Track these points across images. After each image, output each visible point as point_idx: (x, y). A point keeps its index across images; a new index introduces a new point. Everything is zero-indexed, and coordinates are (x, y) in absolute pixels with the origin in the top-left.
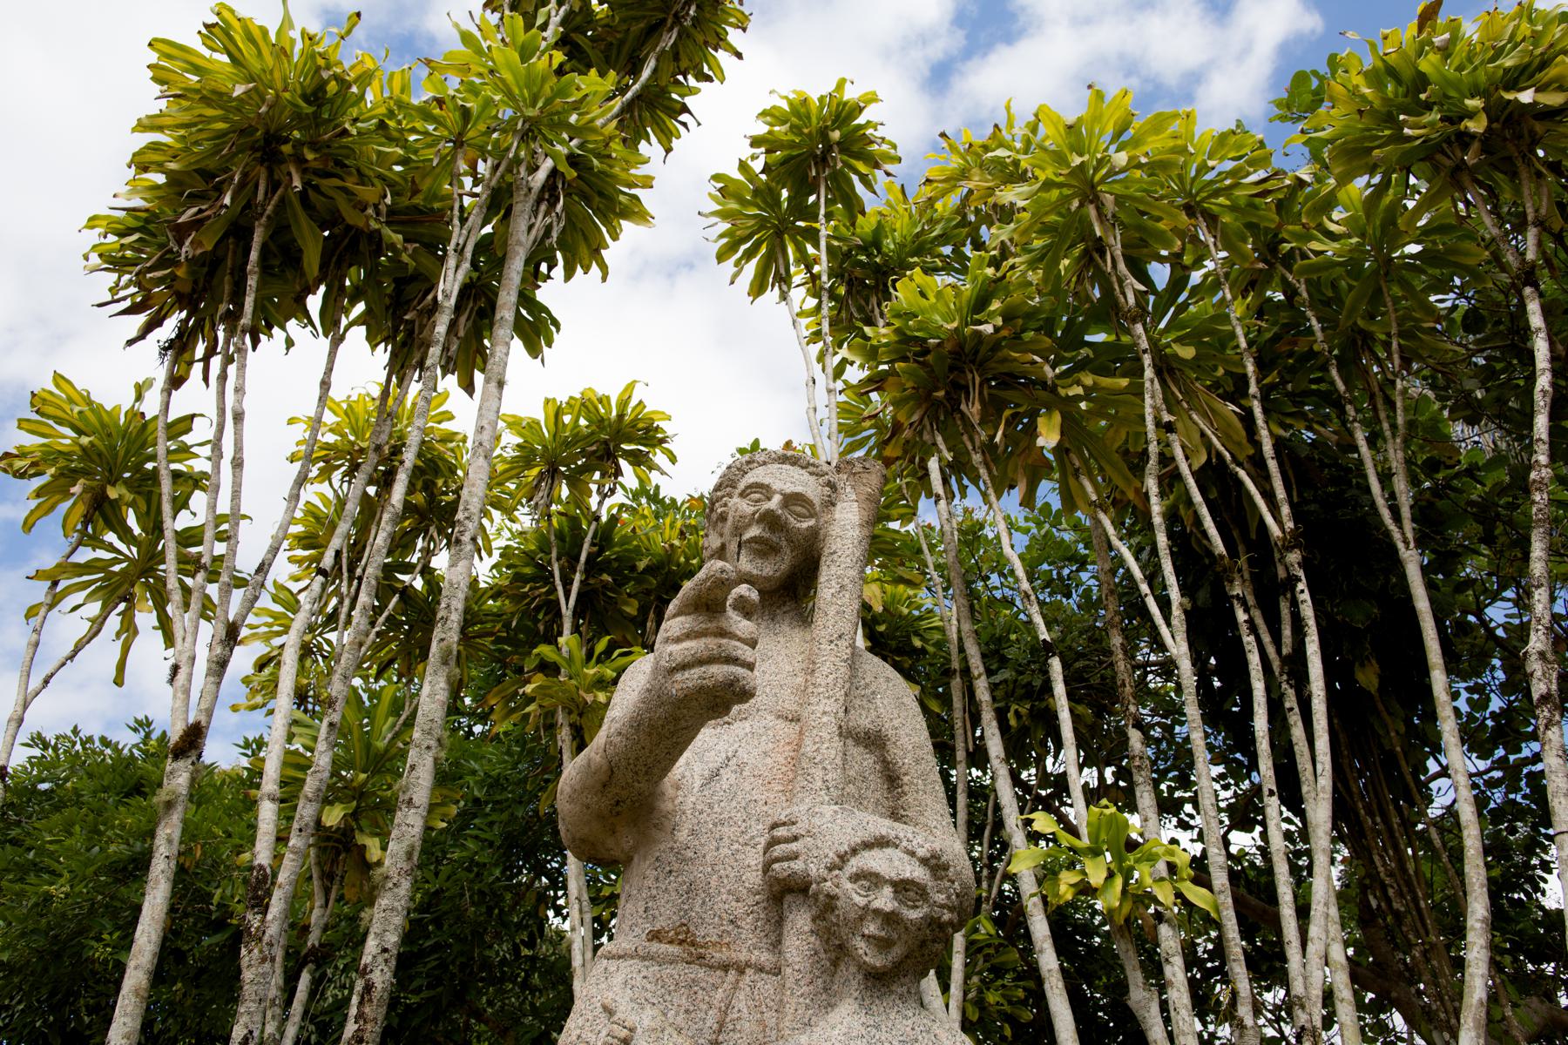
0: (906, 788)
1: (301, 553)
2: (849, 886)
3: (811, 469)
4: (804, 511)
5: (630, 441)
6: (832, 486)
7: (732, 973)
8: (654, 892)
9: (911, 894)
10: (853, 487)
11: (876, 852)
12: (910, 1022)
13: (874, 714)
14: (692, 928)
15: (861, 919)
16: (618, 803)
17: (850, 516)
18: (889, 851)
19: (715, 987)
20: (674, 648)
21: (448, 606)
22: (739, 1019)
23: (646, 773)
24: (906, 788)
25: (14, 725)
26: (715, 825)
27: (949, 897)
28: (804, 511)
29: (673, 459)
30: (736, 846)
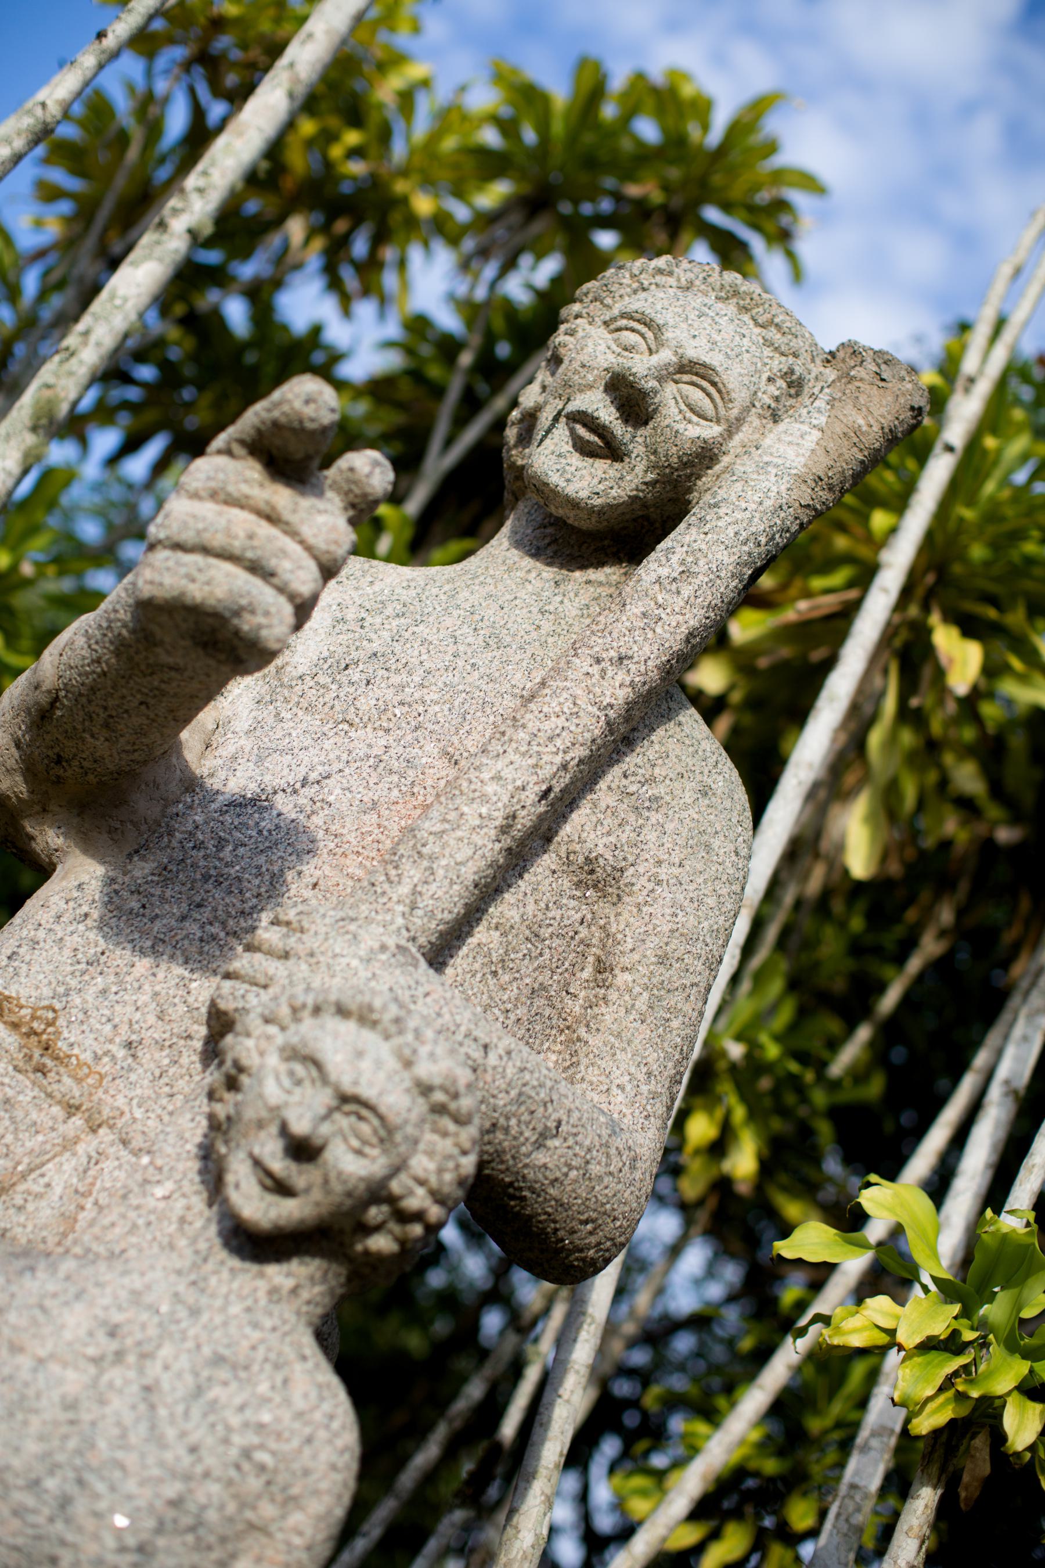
0: (613, 995)
1: (58, 176)
2: (273, 1060)
3: (772, 334)
4: (706, 404)
5: (727, 207)
6: (795, 385)
7: (78, 1121)
8: (41, 934)
9: (365, 1128)
10: (831, 402)
11: (349, 1028)
12: (256, 1335)
13: (627, 834)
14: (61, 1022)
15: (260, 1125)
16: (59, 760)
17: (791, 453)
18: (369, 1038)
19: (35, 1128)
20: (208, 509)
21: (86, 333)
22: (39, 1196)
23: (106, 725)
24: (613, 995)
25: (267, 510)
26: (206, 878)
27: (440, 1171)
28: (706, 404)
29: (797, 273)
30: (215, 929)
